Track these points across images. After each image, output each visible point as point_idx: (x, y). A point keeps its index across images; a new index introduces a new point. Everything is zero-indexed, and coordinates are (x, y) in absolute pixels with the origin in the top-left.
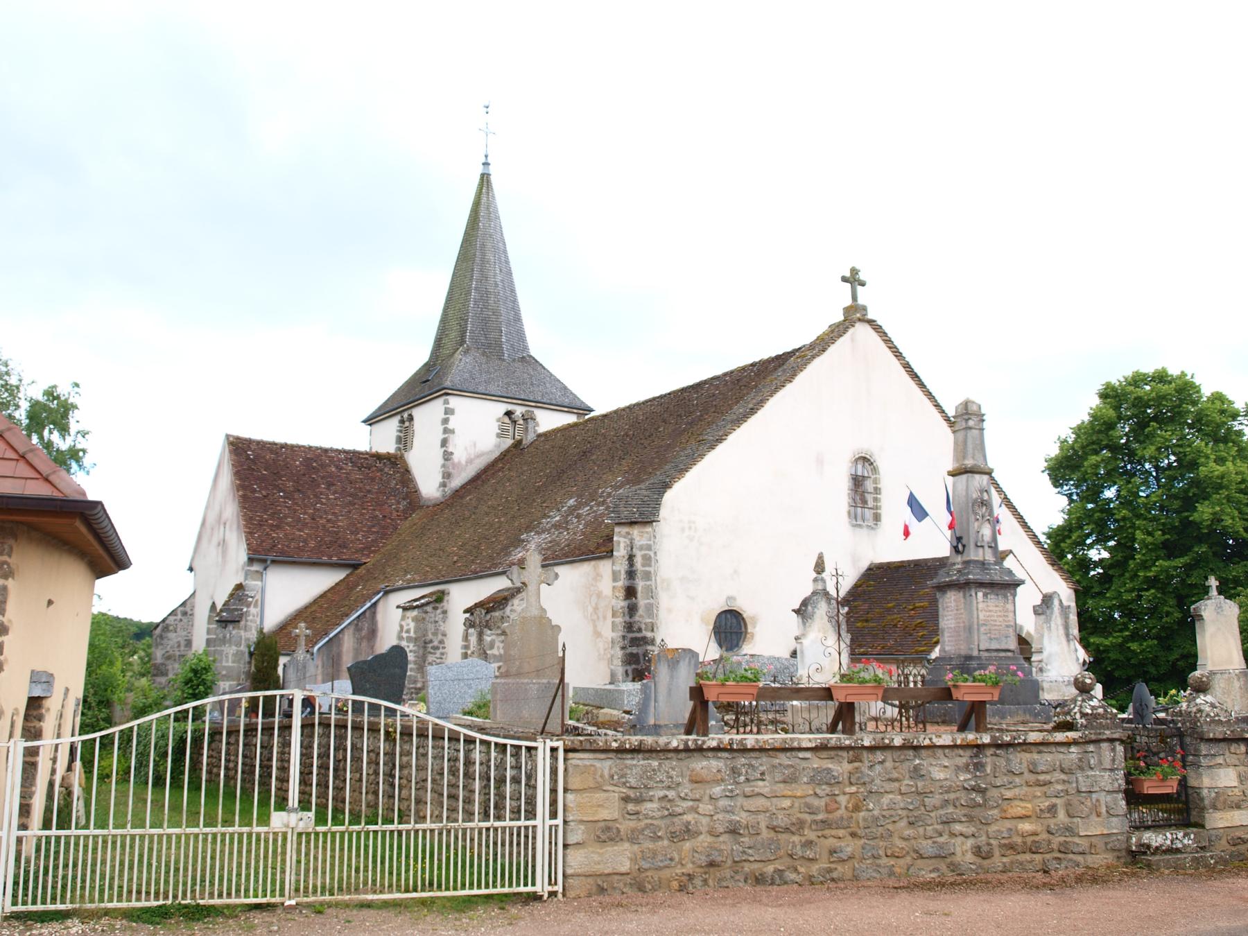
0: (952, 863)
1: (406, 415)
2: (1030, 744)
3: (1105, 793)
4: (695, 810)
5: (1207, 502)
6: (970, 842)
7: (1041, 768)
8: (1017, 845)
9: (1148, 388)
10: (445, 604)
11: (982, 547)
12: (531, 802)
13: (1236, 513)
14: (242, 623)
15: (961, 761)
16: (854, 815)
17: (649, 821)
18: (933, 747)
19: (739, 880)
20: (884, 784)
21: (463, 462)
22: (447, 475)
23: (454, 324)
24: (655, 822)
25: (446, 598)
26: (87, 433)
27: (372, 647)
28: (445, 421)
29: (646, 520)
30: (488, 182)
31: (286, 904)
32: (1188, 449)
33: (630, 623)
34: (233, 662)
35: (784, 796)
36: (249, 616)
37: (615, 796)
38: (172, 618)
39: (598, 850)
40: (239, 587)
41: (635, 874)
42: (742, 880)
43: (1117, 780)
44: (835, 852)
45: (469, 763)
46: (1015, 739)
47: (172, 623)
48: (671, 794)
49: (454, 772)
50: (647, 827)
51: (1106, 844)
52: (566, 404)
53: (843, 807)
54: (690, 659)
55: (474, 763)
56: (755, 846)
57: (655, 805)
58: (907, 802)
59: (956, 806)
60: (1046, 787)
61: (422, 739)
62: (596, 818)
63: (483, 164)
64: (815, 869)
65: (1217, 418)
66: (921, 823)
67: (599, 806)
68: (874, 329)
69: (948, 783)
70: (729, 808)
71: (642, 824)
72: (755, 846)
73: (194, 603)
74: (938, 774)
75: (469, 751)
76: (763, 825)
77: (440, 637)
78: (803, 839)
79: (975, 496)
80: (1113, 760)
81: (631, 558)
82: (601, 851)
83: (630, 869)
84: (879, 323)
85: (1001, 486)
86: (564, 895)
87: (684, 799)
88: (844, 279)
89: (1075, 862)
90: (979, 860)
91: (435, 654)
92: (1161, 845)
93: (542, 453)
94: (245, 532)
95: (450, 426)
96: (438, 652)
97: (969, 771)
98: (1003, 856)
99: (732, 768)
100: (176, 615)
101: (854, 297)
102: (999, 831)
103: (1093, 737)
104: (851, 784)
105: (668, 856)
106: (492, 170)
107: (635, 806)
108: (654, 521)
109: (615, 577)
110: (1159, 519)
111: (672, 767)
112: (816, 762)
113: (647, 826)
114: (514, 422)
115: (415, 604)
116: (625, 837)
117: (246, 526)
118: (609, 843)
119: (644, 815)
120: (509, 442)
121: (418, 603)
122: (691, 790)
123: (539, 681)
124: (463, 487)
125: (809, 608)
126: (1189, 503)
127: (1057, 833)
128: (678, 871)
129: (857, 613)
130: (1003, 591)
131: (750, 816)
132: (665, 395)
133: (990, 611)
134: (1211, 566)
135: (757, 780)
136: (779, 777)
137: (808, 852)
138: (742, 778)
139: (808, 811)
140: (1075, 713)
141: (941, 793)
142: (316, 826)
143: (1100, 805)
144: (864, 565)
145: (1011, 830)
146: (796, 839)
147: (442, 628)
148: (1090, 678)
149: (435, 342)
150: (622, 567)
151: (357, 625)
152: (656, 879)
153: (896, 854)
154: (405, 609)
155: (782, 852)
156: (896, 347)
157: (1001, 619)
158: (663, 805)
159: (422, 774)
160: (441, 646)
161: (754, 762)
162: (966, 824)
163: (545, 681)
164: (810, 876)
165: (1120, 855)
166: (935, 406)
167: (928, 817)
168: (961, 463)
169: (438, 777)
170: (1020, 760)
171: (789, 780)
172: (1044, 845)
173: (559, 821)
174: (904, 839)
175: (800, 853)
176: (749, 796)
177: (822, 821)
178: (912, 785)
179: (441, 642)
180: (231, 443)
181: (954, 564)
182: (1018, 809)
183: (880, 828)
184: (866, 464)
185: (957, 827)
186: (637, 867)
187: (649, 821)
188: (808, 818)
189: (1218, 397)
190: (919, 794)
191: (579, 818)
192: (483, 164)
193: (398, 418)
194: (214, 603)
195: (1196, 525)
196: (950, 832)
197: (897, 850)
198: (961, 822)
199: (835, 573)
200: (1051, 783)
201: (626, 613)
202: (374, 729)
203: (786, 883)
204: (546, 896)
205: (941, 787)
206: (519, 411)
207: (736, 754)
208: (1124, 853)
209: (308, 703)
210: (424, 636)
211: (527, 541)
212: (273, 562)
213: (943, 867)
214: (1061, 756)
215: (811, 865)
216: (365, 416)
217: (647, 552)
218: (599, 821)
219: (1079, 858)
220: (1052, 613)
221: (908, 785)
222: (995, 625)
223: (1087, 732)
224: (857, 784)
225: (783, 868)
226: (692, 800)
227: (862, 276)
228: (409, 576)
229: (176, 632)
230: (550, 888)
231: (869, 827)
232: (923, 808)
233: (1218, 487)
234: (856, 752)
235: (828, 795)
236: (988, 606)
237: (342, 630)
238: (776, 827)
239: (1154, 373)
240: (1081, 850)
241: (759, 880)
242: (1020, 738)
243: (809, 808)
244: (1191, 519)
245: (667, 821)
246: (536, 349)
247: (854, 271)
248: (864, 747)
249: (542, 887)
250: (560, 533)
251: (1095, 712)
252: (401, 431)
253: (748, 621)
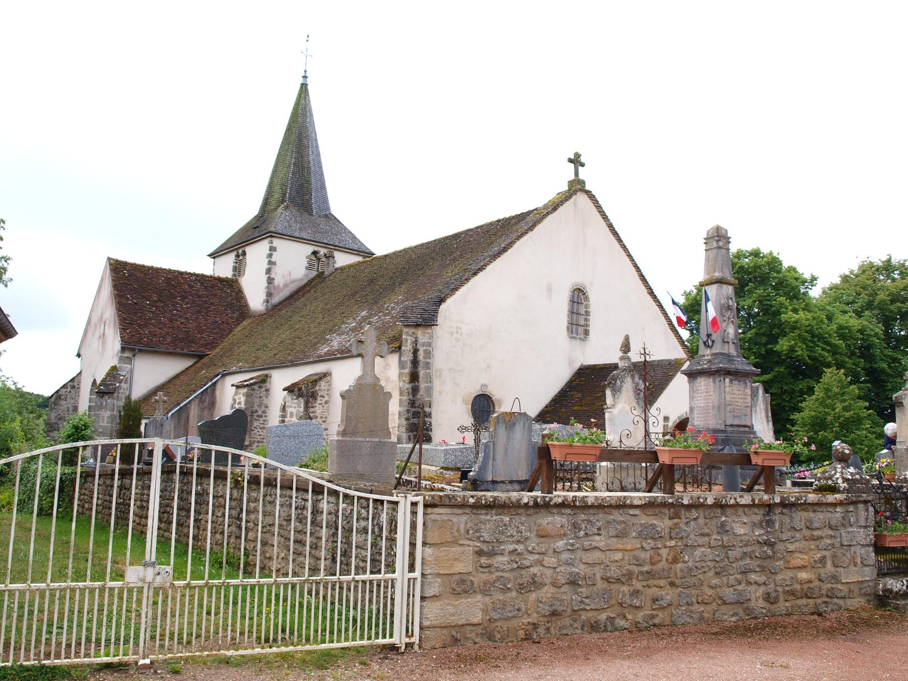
0: (748, 608)
1: (240, 251)
2: (809, 504)
3: (860, 546)
4: (540, 563)
5: (785, 338)
6: (762, 590)
7: (816, 525)
8: (797, 591)
9: (747, 260)
10: (268, 384)
11: (728, 342)
12: (391, 555)
13: (804, 346)
14: (115, 395)
15: (757, 518)
16: (672, 566)
17: (500, 574)
18: (737, 505)
19: (577, 628)
20: (698, 539)
21: (282, 286)
22: (269, 295)
23: (277, 188)
24: (505, 575)
25: (269, 380)
26: (9, 259)
27: (212, 415)
28: (270, 256)
29: (428, 324)
30: (306, 89)
31: (139, 664)
32: (774, 302)
33: (414, 401)
34: (108, 423)
35: (616, 550)
36: (121, 389)
37: (469, 550)
38: (64, 390)
39: (453, 602)
40: (114, 368)
41: (486, 625)
42: (579, 628)
43: (869, 535)
44: (657, 600)
45: (316, 511)
46: (798, 499)
47: (64, 393)
48: (520, 548)
49: (301, 520)
50: (498, 580)
51: (860, 589)
52: (355, 249)
53: (664, 559)
54: (524, 422)
55: (322, 512)
56: (591, 596)
57: (505, 559)
58: (715, 555)
59: (752, 558)
60: (818, 541)
61: (270, 488)
62: (452, 572)
63: (303, 77)
64: (640, 616)
65: (795, 283)
66: (725, 573)
67: (455, 559)
68: (590, 197)
69: (747, 538)
70: (570, 561)
71: (494, 576)
72: (591, 596)
73: (80, 379)
74: (740, 530)
75: (317, 501)
76: (598, 577)
77: (263, 408)
78: (632, 589)
79: (723, 302)
80: (867, 519)
81: (415, 352)
82: (456, 603)
83: (482, 620)
84: (594, 193)
85: (669, 315)
86: (420, 647)
87: (531, 553)
88: (570, 161)
89: (838, 605)
90: (768, 605)
91: (259, 420)
92: (900, 590)
93: (340, 280)
94: (120, 328)
95: (273, 259)
96: (262, 419)
97: (762, 527)
98: (786, 601)
99: (574, 523)
100: (66, 388)
101: (577, 174)
102: (784, 579)
103: (854, 499)
104: (671, 538)
105: (516, 607)
106: (309, 81)
107: (487, 560)
108: (433, 325)
109: (402, 365)
110: (753, 349)
111: (522, 523)
112: (644, 519)
113: (499, 578)
114: (319, 259)
115: (245, 383)
116: (477, 590)
117: (120, 324)
118: (464, 595)
119: (496, 567)
120: (314, 273)
121: (248, 383)
122: (538, 544)
123: (372, 440)
124: (281, 303)
125: (618, 382)
126: (774, 339)
127: (826, 580)
128: (524, 621)
129: (573, 400)
130: (743, 379)
131: (587, 568)
133: (734, 394)
134: (785, 381)
135: (594, 534)
136: (612, 532)
137: (635, 601)
138: (582, 533)
139: (636, 563)
140: (838, 478)
141: (741, 547)
142: (174, 580)
143: (856, 557)
144: (577, 366)
145: (793, 578)
146: (625, 588)
147: (265, 402)
148: (848, 449)
149: (263, 201)
150: (408, 357)
151: (201, 398)
152: (505, 629)
153: (706, 601)
154: (238, 387)
155: (613, 602)
156: (604, 212)
157: (742, 401)
158: (513, 558)
159: (269, 520)
160: (264, 415)
161: (592, 518)
162: (759, 574)
163: (377, 440)
164: (636, 622)
165: (870, 599)
166: (628, 256)
167: (730, 568)
168: (711, 275)
169: (284, 523)
170: (800, 518)
171: (621, 535)
172: (817, 590)
173: (417, 574)
174: (712, 587)
175: (628, 602)
176: (587, 550)
177: (647, 572)
178: (719, 539)
179: (264, 412)
180: (111, 264)
181: (704, 356)
182: (798, 560)
183: (693, 578)
184: (581, 294)
185: (752, 576)
186: (488, 617)
187: (500, 574)
188: (636, 569)
189: (792, 269)
190: (724, 547)
191: (437, 571)
192: (303, 77)
193: (235, 253)
194: (95, 380)
195: (778, 354)
196: (747, 580)
197: (707, 597)
198: (756, 572)
199: (643, 352)
200: (822, 537)
201: (411, 393)
202: (221, 476)
203: (616, 629)
204: (403, 647)
205: (741, 541)
206: (322, 251)
207: (577, 511)
208: (872, 598)
209: (168, 454)
210: (252, 407)
211: (331, 340)
212: (140, 351)
213: (741, 613)
214: (830, 515)
215: (637, 612)
216: (210, 252)
217: (427, 348)
218: (454, 574)
219: (841, 602)
220: (757, 400)
221: (716, 539)
222: (737, 405)
223: (850, 495)
224: (676, 538)
225: (614, 615)
226: (538, 553)
227: (583, 160)
228: (241, 364)
229: (66, 400)
230: (407, 640)
231: (684, 577)
232: (726, 560)
233: (793, 328)
234: (676, 508)
235: (652, 548)
236: (732, 390)
237: (190, 401)
238: (610, 578)
239: (752, 251)
240: (843, 595)
241: (594, 627)
242: (802, 499)
243: (637, 561)
244: (774, 349)
245: (515, 573)
246: (336, 210)
247: (577, 156)
248: (683, 505)
249: (398, 638)
250: (356, 335)
251: (854, 478)
252: (236, 263)
253: (496, 403)
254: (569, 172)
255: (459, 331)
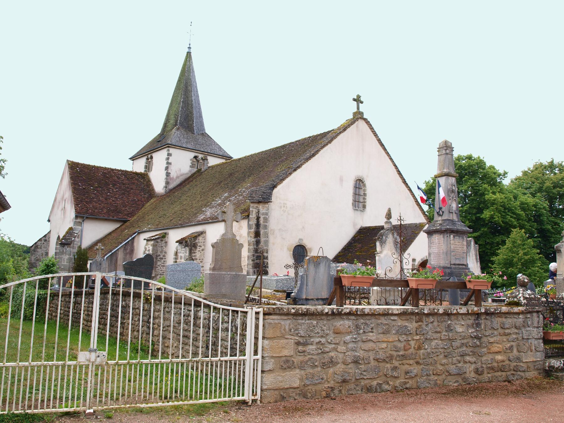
0: (464, 378)
1: (149, 156)
2: (503, 313)
3: (534, 339)
4: (335, 349)
5: (488, 210)
6: (473, 366)
7: (507, 326)
8: (495, 367)
9: (464, 162)
10: (166, 239)
11: (452, 213)
12: (243, 345)
13: (500, 215)
14: (72, 245)
15: (470, 322)
16: (418, 351)
17: (310, 356)
18: (458, 314)
19: (358, 390)
20: (433, 335)
21: (175, 178)
22: (167, 183)
23: (172, 117)
24: (314, 357)
25: (167, 236)
26: (6, 161)
27: (132, 258)
28: (168, 159)
29: (266, 201)
30: (190, 55)
31: (86, 412)
32: (481, 188)
33: (257, 249)
34: (67, 263)
35: (383, 341)
36: (75, 242)
37: (292, 342)
38: (39, 242)
39: (281, 374)
40: (71, 229)
41: (302, 388)
42: (360, 390)
43: (540, 332)
44: (408, 373)
45: (196, 318)
46: (496, 310)
47: (40, 244)
48: (323, 340)
49: (187, 323)
50: (309, 360)
51: (534, 366)
52: (221, 154)
53: (413, 347)
54: (326, 262)
55: (200, 318)
56: (367, 370)
57: (314, 347)
58: (444, 344)
59: (467, 347)
60: (508, 336)
61: (167, 303)
62: (281, 355)
63: (188, 48)
64: (398, 383)
65: (494, 176)
66: (450, 356)
67: (283, 348)
68: (366, 123)
69: (464, 334)
70: (354, 349)
71: (307, 358)
72: (367, 370)
73: (50, 236)
74: (460, 329)
75: (197, 311)
76: (371, 358)
77: (163, 254)
78: (392, 366)
79: (449, 187)
80: (538, 322)
81: (258, 218)
82: (284, 375)
83: (299, 385)
84: (369, 120)
85: (415, 196)
86: (261, 402)
87: (330, 343)
88: (354, 100)
89: (521, 376)
90: (477, 376)
91: (161, 261)
92: (559, 367)
93: (211, 174)
94: (74, 204)
95: (170, 161)
96: (162, 260)
97: (473, 327)
98: (488, 373)
99: (356, 325)
100: (41, 241)
101: (358, 108)
102: (487, 360)
103: (531, 310)
104: (417, 334)
105: (321, 377)
106: (192, 51)
107: (303, 348)
108: (269, 202)
109: (249, 227)
110: (467, 217)
111: (324, 325)
112: (400, 322)
113: (310, 359)
114: (198, 161)
115: (152, 238)
116: (296, 366)
117: (75, 201)
118: (288, 369)
119: (308, 352)
120: (195, 170)
121: (154, 238)
122: (334, 338)
123: (231, 273)
124: (174, 188)
125: (384, 237)
126: (481, 211)
127: (513, 360)
128: (325, 386)
129: (356, 248)
130: (462, 235)
131: (365, 353)
132: (268, 150)
133: (456, 245)
134: (488, 237)
135: (369, 332)
136: (380, 331)
137: (394, 373)
138: (362, 331)
139: (395, 350)
140: (520, 297)
141: (460, 340)
142: (108, 360)
143: (532, 346)
144: (358, 227)
145: (492, 359)
146: (388, 365)
147: (164, 250)
148: (527, 279)
150: (253, 222)
151: (125, 247)
152: (313, 390)
153: (438, 373)
154: (148, 240)
155: (381, 374)
156: (375, 132)
157: (461, 249)
158: (318, 347)
159: (167, 323)
160: (164, 258)
161: (368, 322)
162: (471, 356)
163: (234, 273)
164: (395, 386)
165: (540, 372)
166: (390, 159)
167: (454, 353)
168: (442, 171)
169: (177, 325)
170: (497, 322)
171: (386, 332)
172: (507, 366)
173: (259, 356)
174: (442, 365)
175: (390, 374)
176: (365, 342)
177: (402, 356)
178: (446, 335)
179: (164, 256)
180: (69, 164)
181: (437, 221)
182: (496, 348)
183: (431, 359)
184: (361, 182)
185: (467, 358)
186: (303, 384)
187: (310, 356)
188: (395, 354)
189: (492, 167)
190: (449, 340)
191: (271, 355)
193: (146, 157)
194: (59, 236)
195: (483, 220)
196: (464, 361)
197: (439, 371)
198: (469, 355)
199: (399, 219)
200: (511, 334)
201: (255, 244)
202: (137, 296)
203: (383, 391)
204: (251, 402)
205: (460, 336)
206: (200, 156)
207: (358, 317)
208: (542, 371)
210: (156, 253)
211: (206, 211)
212: (87, 218)
213: (460, 380)
214: (515, 320)
215: (396, 380)
217: (265, 216)
218: (282, 356)
219: (522, 374)
220: (470, 248)
221: (445, 335)
222: (458, 252)
223: (528, 307)
224: (420, 334)
225: (381, 382)
226: (334, 344)
227: (362, 99)
228: (149, 226)
229: (41, 249)
230: (253, 398)
231: (425, 359)
232: (451, 348)
233: (493, 204)
234: (420, 316)
235: (405, 341)
236: (455, 242)
237: (118, 249)
238: (379, 359)
240: (523, 369)
241: (369, 390)
242: (498, 310)
243: (396, 348)
244: (481, 217)
245: (320, 356)
246: (208, 130)
247: (359, 97)
248: (424, 314)
249: (247, 396)
250: (221, 208)
251: (530, 297)
252: (147, 163)
253: (308, 250)
254: (353, 107)
255: (285, 205)
